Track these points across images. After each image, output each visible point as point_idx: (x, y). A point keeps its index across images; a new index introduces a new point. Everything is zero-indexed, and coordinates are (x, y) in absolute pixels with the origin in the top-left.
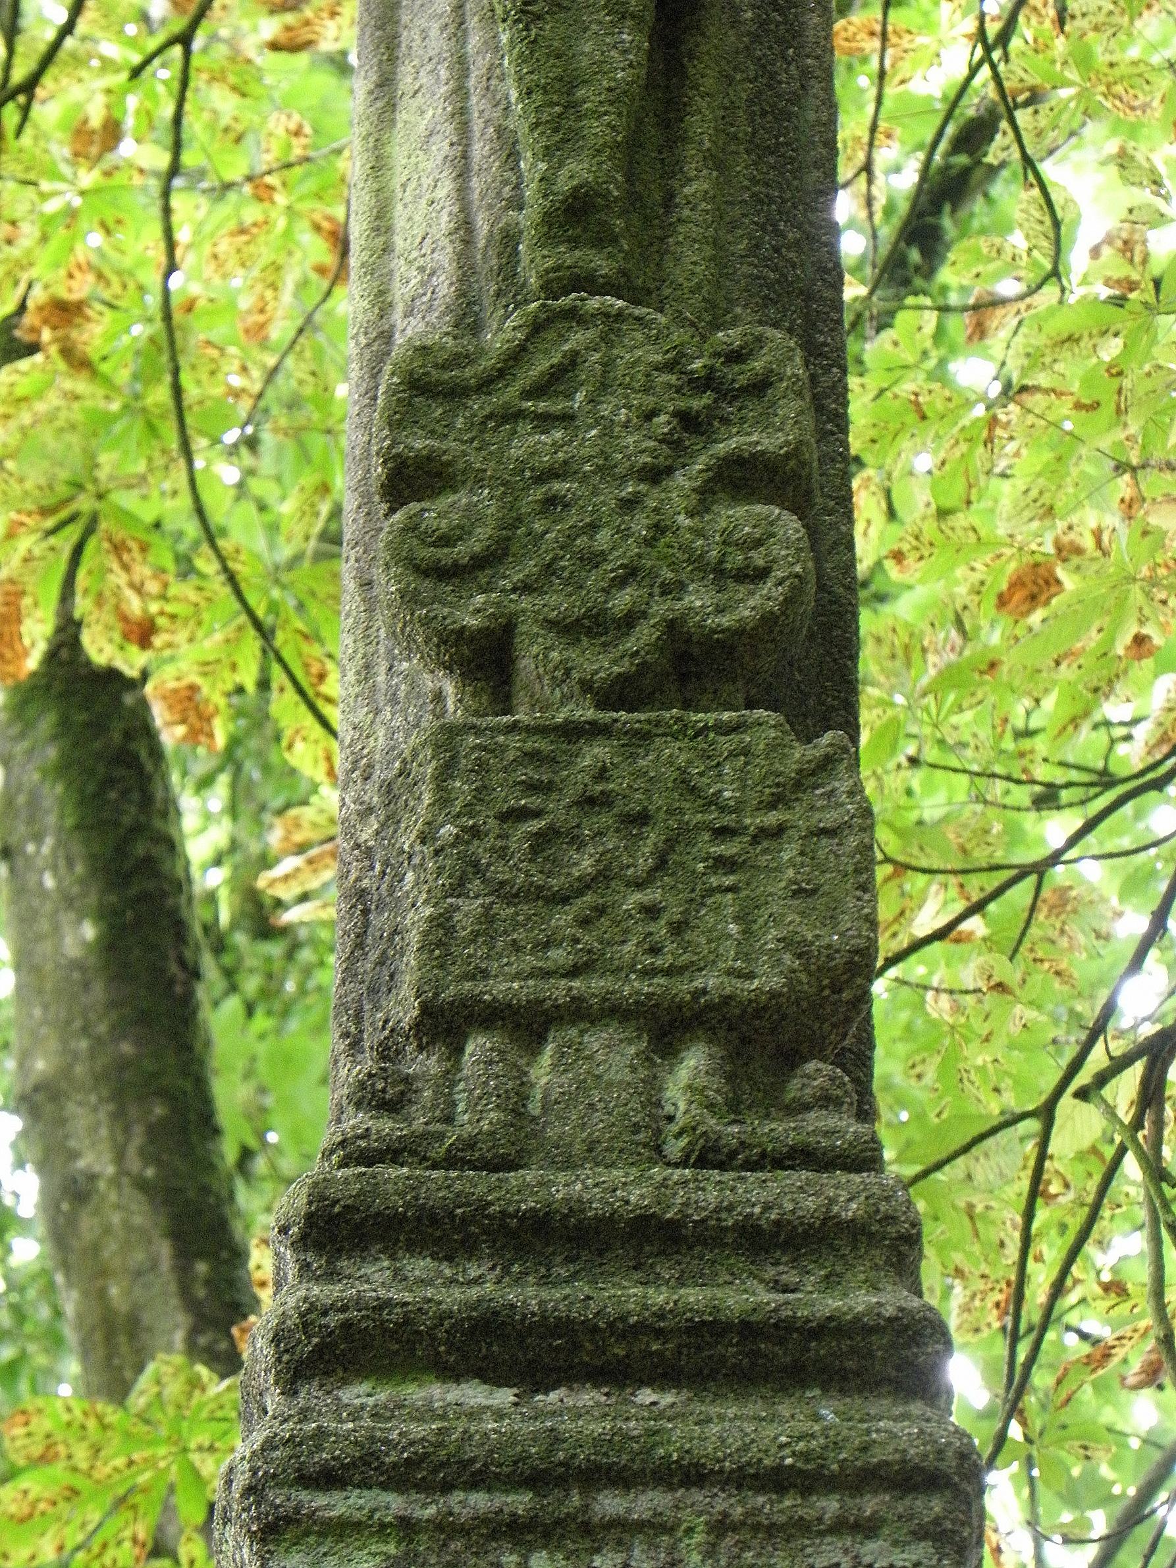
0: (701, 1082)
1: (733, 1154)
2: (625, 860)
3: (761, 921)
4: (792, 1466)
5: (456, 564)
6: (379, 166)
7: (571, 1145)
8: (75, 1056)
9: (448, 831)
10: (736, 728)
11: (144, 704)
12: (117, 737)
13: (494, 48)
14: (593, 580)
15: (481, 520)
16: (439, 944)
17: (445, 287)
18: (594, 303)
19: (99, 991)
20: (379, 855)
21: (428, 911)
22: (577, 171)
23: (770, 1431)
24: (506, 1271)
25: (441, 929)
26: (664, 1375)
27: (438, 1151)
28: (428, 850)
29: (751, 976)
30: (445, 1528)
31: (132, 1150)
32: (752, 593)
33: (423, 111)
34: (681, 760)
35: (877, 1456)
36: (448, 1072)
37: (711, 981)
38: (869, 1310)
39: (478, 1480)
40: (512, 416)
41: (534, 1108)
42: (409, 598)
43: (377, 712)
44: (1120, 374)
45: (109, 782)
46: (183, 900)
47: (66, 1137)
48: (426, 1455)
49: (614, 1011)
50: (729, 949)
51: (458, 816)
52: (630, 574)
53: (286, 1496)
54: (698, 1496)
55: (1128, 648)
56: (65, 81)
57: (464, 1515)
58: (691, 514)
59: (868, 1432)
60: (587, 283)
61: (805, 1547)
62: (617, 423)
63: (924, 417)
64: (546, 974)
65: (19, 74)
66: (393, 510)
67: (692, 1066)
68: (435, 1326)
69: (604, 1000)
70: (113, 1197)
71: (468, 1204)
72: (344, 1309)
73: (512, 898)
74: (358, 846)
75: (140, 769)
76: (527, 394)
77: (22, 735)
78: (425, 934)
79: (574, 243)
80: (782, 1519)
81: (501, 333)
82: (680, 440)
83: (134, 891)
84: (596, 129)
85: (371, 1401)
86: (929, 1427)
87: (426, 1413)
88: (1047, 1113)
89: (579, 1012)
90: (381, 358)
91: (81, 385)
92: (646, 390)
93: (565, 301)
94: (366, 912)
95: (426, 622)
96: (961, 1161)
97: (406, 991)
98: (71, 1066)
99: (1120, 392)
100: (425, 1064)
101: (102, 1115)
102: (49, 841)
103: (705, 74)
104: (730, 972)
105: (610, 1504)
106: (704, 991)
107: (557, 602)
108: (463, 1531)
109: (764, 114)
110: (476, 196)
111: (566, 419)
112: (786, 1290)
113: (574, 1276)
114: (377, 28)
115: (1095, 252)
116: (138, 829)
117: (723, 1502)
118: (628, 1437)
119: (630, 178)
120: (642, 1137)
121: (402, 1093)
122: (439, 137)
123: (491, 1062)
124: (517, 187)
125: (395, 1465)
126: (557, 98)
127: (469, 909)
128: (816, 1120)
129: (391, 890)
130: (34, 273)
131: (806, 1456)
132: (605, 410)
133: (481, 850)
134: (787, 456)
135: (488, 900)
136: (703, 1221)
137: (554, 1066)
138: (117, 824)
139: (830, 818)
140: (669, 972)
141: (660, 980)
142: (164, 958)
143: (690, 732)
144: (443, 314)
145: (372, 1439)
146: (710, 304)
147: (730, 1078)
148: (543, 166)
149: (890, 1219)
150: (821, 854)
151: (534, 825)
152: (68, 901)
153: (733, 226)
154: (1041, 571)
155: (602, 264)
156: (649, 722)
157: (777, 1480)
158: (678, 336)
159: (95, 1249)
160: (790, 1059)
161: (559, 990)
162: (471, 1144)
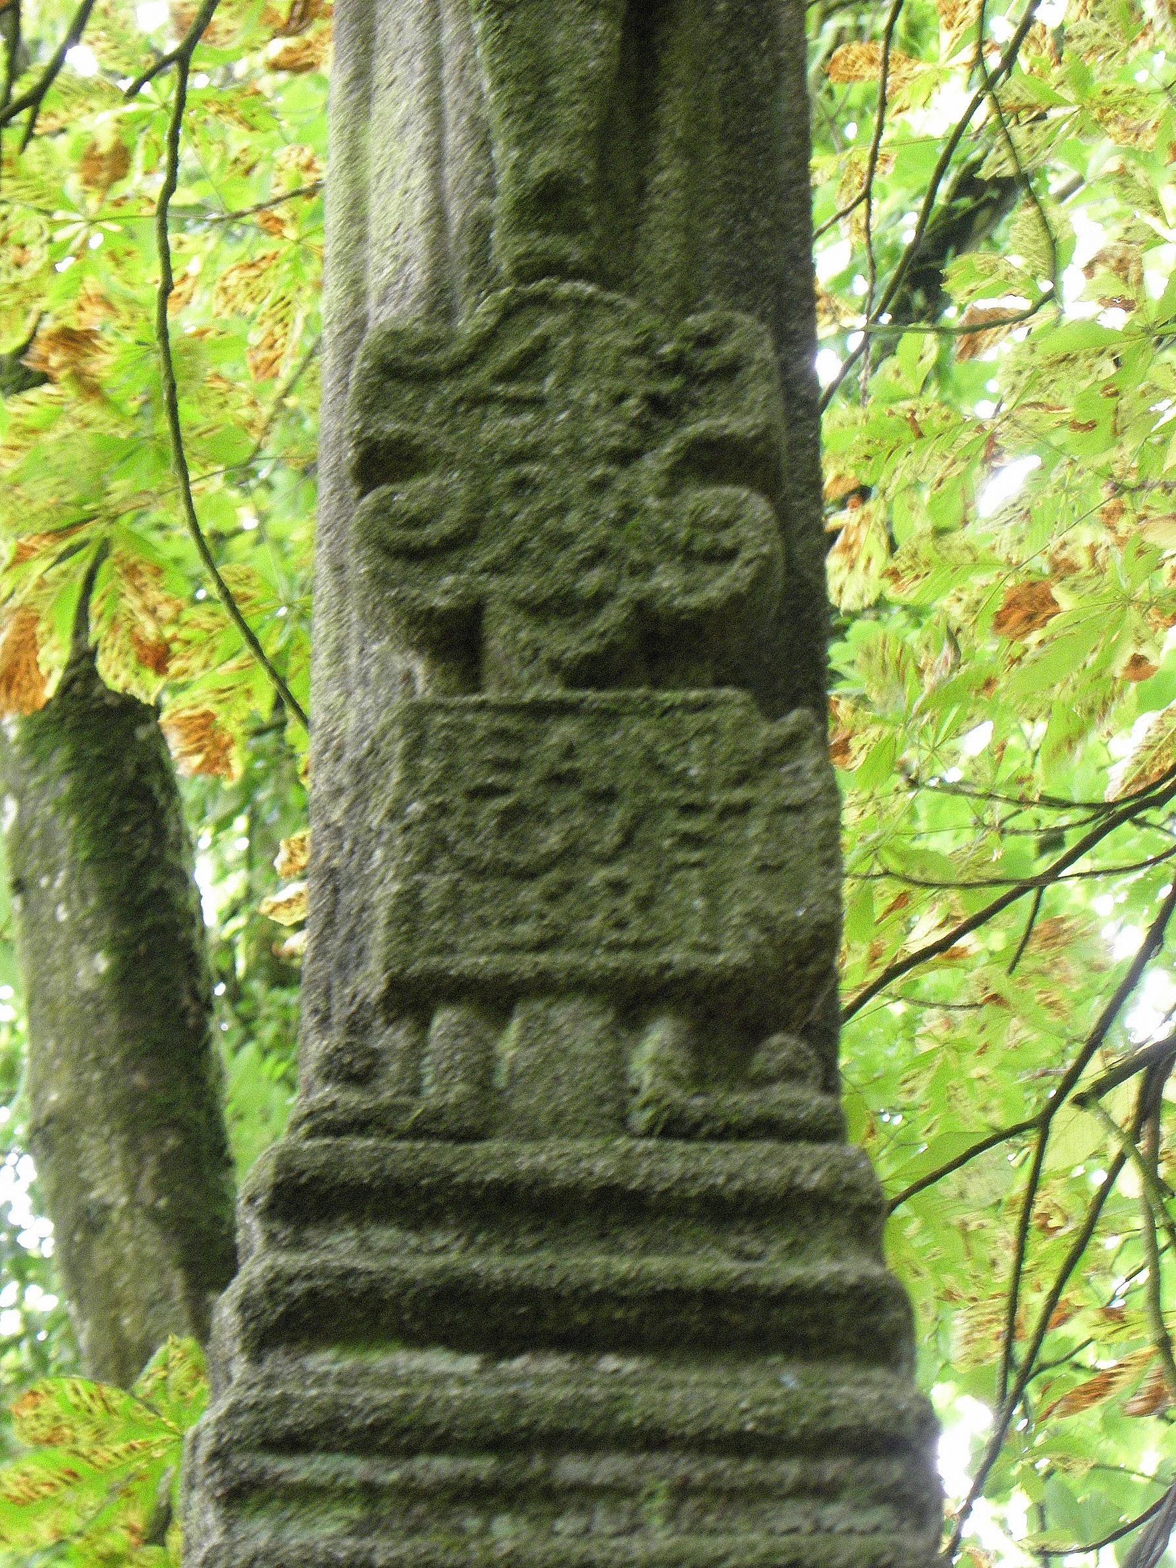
0: (667, 1054)
1: (698, 1126)
2: (592, 837)
3: (726, 897)
4: (752, 1432)
5: (425, 546)
6: (354, 157)
7: (535, 1117)
8: (88, 1088)
9: (416, 808)
11: (159, 737)
12: (130, 771)
13: (468, 37)
14: (563, 561)
15: (450, 502)
16: (406, 920)
17: (418, 274)
18: (565, 289)
19: (111, 1023)
20: (349, 833)
21: (396, 887)
22: (548, 159)
23: (732, 1396)
24: (471, 1242)
25: (409, 906)
26: (627, 1342)
27: (405, 1123)
28: (397, 826)
29: (716, 950)
30: (408, 1492)
31: (145, 1180)
32: (719, 574)
33: (399, 101)
34: (649, 737)
35: (838, 1421)
36: (414, 1047)
37: (677, 956)
38: (832, 1277)
39: (442, 1444)
40: (481, 400)
41: (501, 1080)
42: (380, 579)
43: (349, 694)
44: (1116, 394)
45: (122, 815)
46: (196, 932)
47: (79, 1169)
48: (389, 1422)
49: (581, 986)
50: (695, 925)
51: (426, 794)
52: (599, 555)
53: (252, 1469)
54: (660, 1461)
55: (1126, 669)
56: (76, 111)
58: (661, 495)
59: (828, 1397)
60: (558, 269)
61: (764, 1512)
62: (586, 408)
63: (920, 435)
64: (512, 949)
65: (20, 90)
66: (363, 494)
67: (659, 1037)
68: (399, 1295)
69: (570, 975)
70: (126, 1227)
71: (432, 1174)
72: (309, 1277)
73: (480, 874)
74: (327, 826)
75: (154, 801)
76: (499, 378)
77: (36, 768)
78: (394, 909)
79: (546, 230)
80: (742, 1483)
81: (473, 317)
82: (649, 424)
83: (147, 923)
85: (336, 1368)
86: (892, 1392)
87: (390, 1380)
88: (1043, 1123)
89: (545, 986)
90: (354, 345)
91: (91, 411)
92: (617, 373)
94: (336, 890)
95: (397, 602)
96: (952, 1175)
98: (83, 1098)
99: (1116, 411)
100: (392, 1038)
101: (114, 1147)
102: (62, 875)
103: (678, 63)
104: (696, 947)
105: (572, 1468)
106: (668, 966)
109: (736, 104)
110: (449, 184)
111: (536, 402)
112: (749, 1257)
113: (538, 1246)
114: (352, 23)
115: (1090, 269)
116: (150, 863)
117: (685, 1467)
118: (590, 1404)
119: (603, 167)
120: (608, 1108)
121: (369, 1067)
122: (413, 127)
123: (457, 1036)
124: (489, 175)
125: (359, 1431)
126: (529, 85)
127: (437, 884)
128: (781, 1092)
129: (361, 867)
130: (42, 304)
131: (767, 1421)
132: (575, 393)
133: (449, 827)
134: (756, 440)
135: (457, 876)
136: (666, 1192)
137: (521, 1039)
138: (129, 857)
139: (795, 795)
140: (637, 946)
141: (626, 955)
142: (176, 989)
143: (657, 711)
144: (415, 302)
145: (337, 1406)
146: (682, 291)
147: (697, 1051)
148: (515, 154)
149: (852, 1189)
150: (788, 830)
151: (502, 803)
152: (82, 934)
153: (706, 213)
154: (1037, 590)
155: (574, 251)
156: (615, 700)
157: (738, 1445)
158: (648, 321)
159: (109, 1278)
160: (755, 1033)
161: (526, 965)
162: (437, 1115)
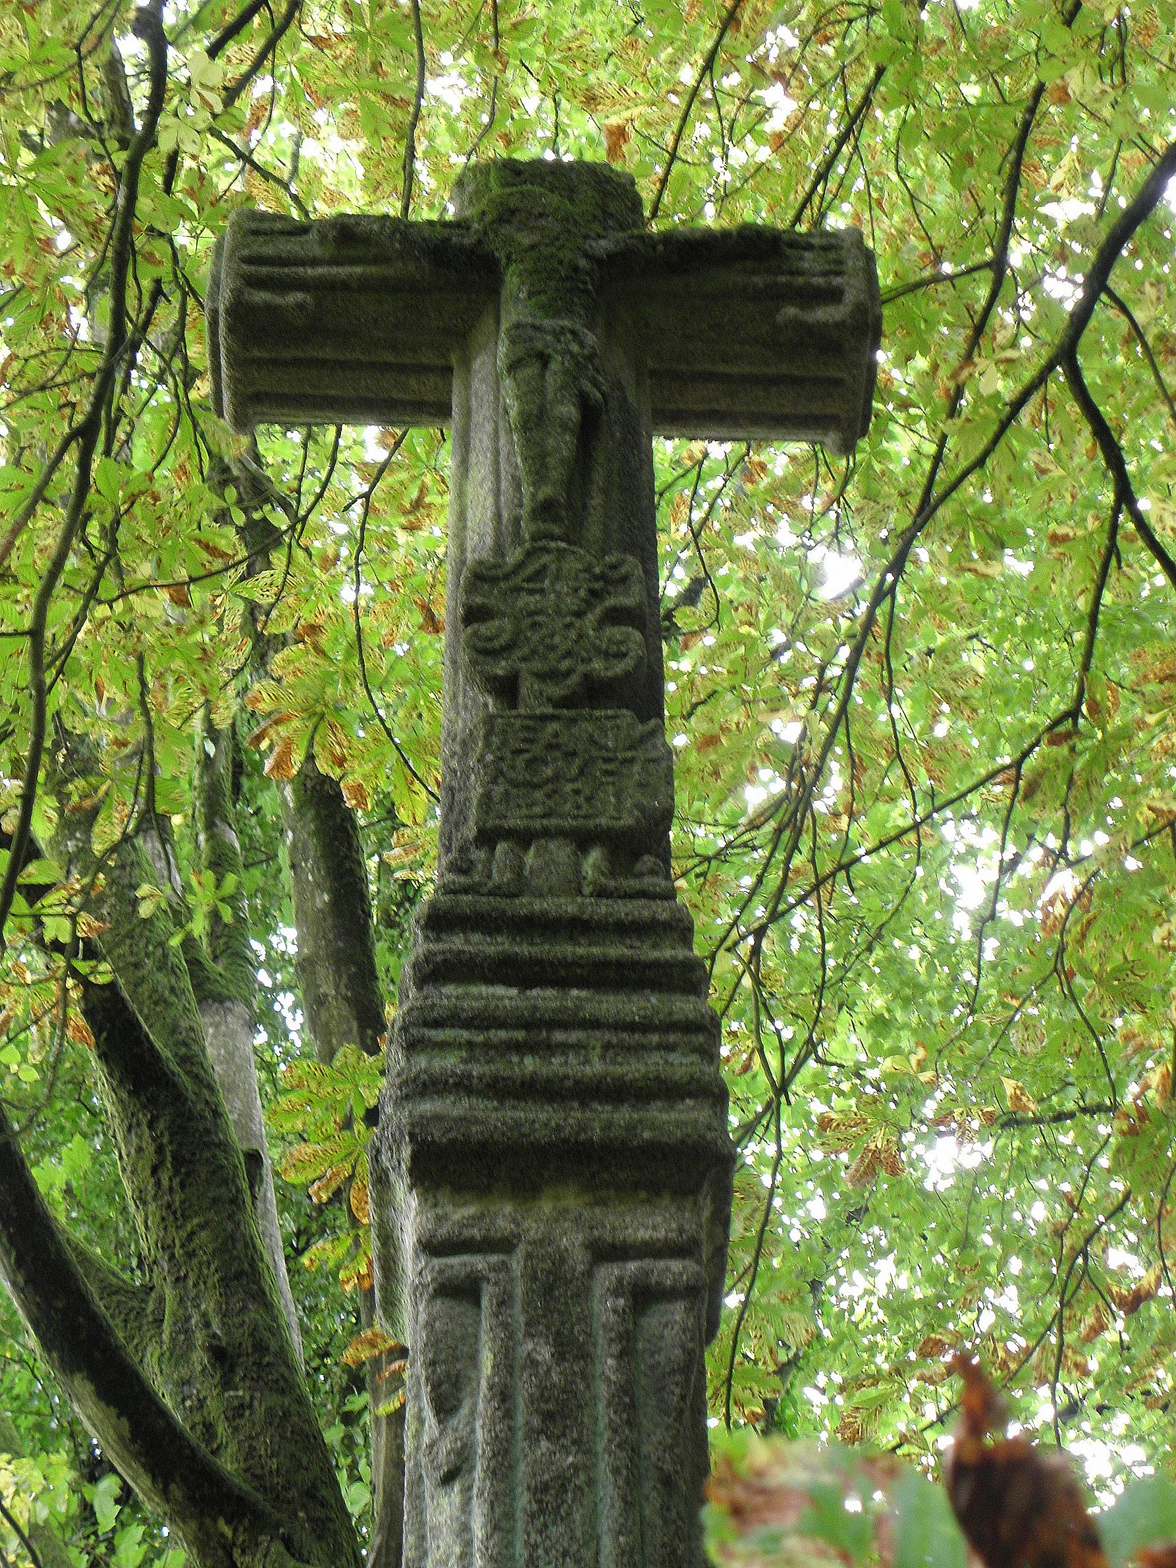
9: (489, 757)
10: (615, 717)
14: (552, 656)
17: (489, 541)
18: (553, 545)
19: (330, 921)
22: (546, 491)
25: (487, 798)
26: (582, 984)
27: (485, 890)
30: (487, 1045)
33: (481, 470)
35: (675, 1017)
37: (603, 821)
39: (502, 1025)
41: (526, 873)
42: (474, 663)
49: (561, 833)
52: (569, 654)
54: (598, 1034)
57: (495, 1040)
60: (552, 537)
62: (563, 593)
64: (530, 817)
73: (516, 785)
81: (513, 556)
84: (555, 475)
87: (480, 997)
89: (546, 833)
93: (541, 544)
97: (471, 823)
105: (559, 1036)
107: (537, 665)
108: (495, 1047)
111: (542, 591)
116: (346, 857)
117: (608, 1036)
126: (538, 462)
127: (498, 790)
139: (654, 755)
140: (586, 817)
151: (527, 756)
155: (557, 530)
157: (632, 1027)
160: (636, 856)
161: (537, 824)
162: (499, 887)
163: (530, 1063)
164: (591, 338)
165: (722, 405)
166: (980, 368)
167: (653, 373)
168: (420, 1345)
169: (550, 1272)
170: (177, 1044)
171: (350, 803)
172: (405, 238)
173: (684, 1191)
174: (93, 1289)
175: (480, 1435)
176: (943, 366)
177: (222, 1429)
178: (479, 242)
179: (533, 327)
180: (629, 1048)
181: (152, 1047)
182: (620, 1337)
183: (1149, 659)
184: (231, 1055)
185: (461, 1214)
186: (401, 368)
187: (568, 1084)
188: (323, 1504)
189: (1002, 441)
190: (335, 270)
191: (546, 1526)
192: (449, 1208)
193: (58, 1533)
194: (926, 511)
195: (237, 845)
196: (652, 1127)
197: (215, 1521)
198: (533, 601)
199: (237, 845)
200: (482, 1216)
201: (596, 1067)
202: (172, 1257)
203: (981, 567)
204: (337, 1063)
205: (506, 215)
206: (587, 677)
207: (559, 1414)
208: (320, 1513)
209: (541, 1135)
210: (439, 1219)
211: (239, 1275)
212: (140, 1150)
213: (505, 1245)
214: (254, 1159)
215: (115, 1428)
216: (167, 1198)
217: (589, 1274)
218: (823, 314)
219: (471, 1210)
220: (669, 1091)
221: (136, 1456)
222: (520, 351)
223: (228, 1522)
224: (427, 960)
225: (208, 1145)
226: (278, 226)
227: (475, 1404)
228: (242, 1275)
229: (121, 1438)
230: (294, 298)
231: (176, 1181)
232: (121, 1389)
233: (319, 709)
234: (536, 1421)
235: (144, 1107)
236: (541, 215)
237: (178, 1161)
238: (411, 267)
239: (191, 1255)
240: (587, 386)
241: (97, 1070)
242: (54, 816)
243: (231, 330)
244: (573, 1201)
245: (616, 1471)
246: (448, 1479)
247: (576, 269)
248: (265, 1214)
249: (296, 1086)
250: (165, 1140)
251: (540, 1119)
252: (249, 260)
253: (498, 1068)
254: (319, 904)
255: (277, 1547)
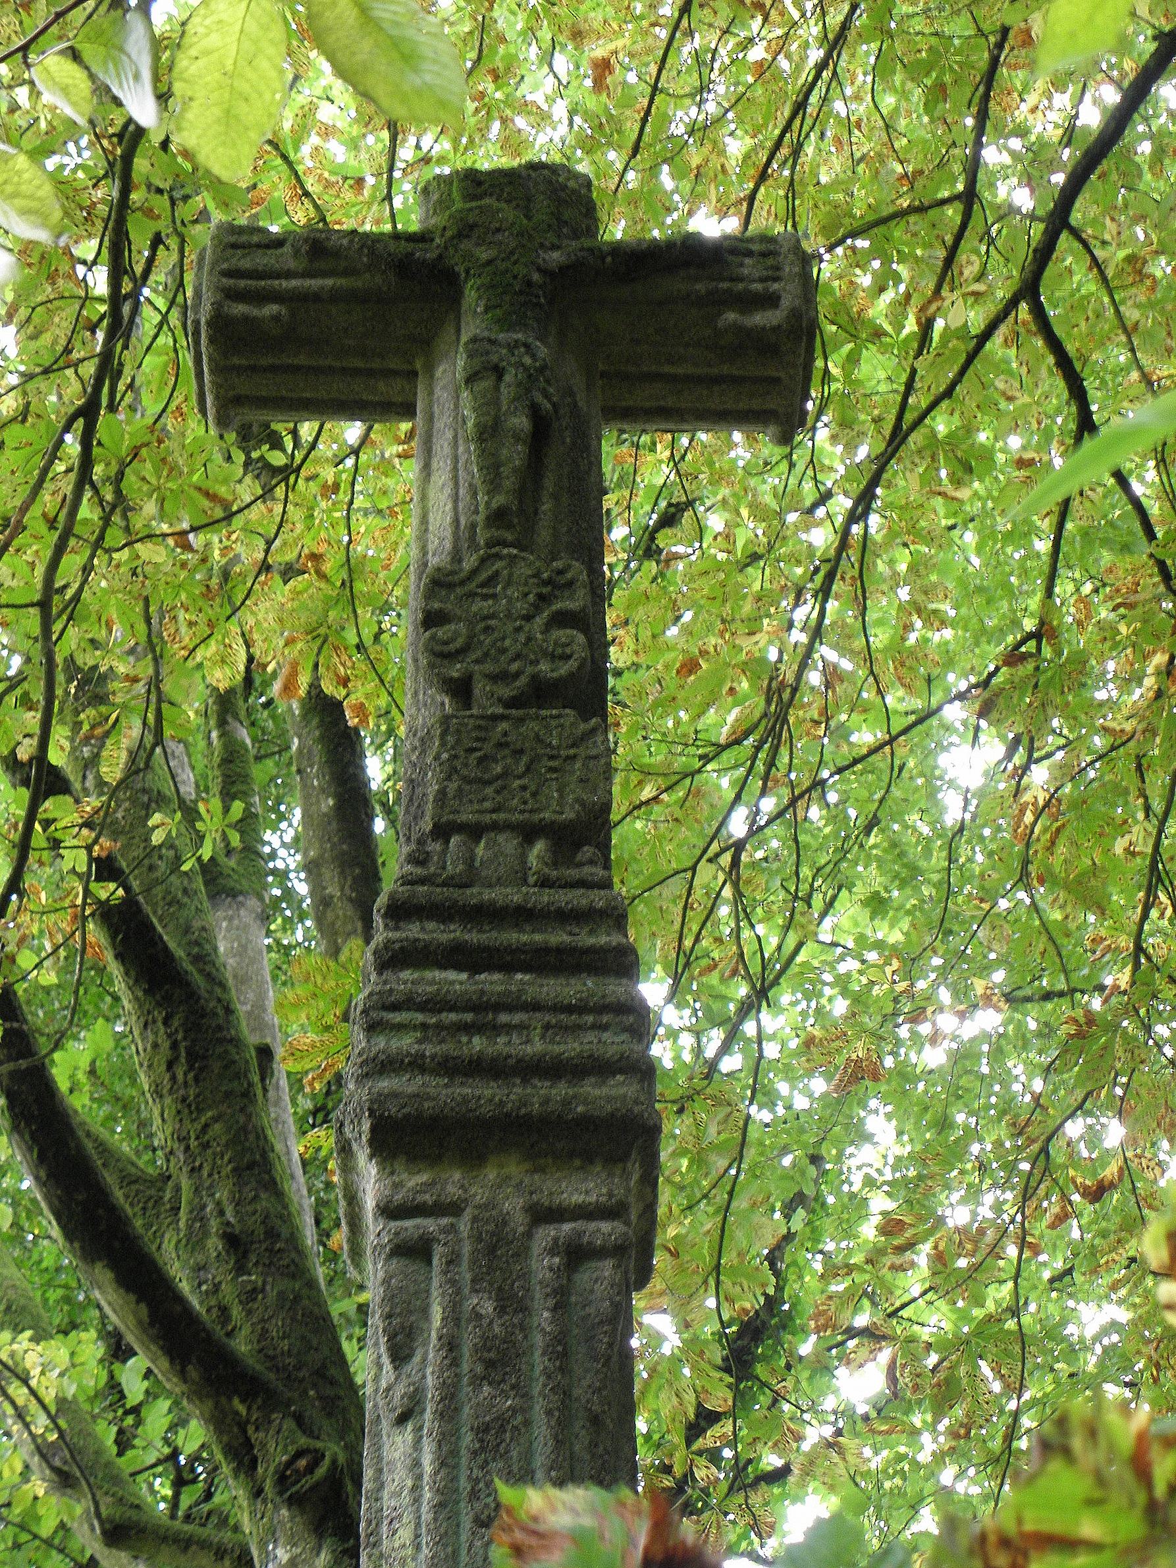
9: (445, 756)
10: (559, 716)
17: (448, 545)
19: (334, 825)
22: (499, 500)
25: (442, 795)
26: (526, 968)
30: (439, 1027)
33: (441, 476)
37: (547, 815)
39: (451, 1009)
42: (431, 666)
49: (508, 827)
52: (518, 656)
60: (505, 544)
62: (513, 598)
73: (470, 782)
81: (469, 562)
84: (507, 484)
87: (432, 982)
89: (495, 827)
97: (428, 818)
105: (504, 1018)
107: (489, 667)
117: (548, 1017)
126: (492, 470)
127: (453, 786)
139: (594, 752)
155: (509, 536)
157: (569, 1009)
160: (578, 846)
161: (487, 818)
163: (478, 1043)
164: (543, 351)
165: (670, 402)
166: (947, 303)
167: (603, 375)
168: (378, 1299)
169: (493, 1234)
170: (189, 943)
171: (352, 722)
172: (372, 253)
173: (615, 1158)
174: (110, 1178)
175: (430, 1381)
176: (915, 296)
177: (236, 1312)
178: (440, 257)
179: (490, 341)
180: (567, 1028)
181: (166, 948)
182: (555, 1292)
183: (1121, 573)
184: (244, 947)
185: (415, 1180)
186: (370, 373)
187: (511, 1062)
188: (333, 1382)
189: (970, 372)
190: (308, 282)
191: (486, 1462)
192: (405, 1176)
193: (86, 1407)
194: (897, 438)
195: (248, 741)
196: (585, 1102)
197: (230, 1399)
198: (485, 606)
199: (248, 741)
200: (433, 1183)
201: (537, 1046)
202: (187, 1148)
203: (949, 489)
204: (343, 958)
205: (465, 230)
206: (534, 678)
207: (499, 1362)
208: (329, 1391)
209: (486, 1110)
210: (396, 1186)
211: (251, 1166)
212: (155, 1046)
213: (454, 1209)
214: (265, 1053)
215: (135, 1313)
216: (182, 1092)
217: (529, 1235)
218: (761, 319)
219: (424, 1178)
220: (601, 1068)
221: (154, 1339)
222: (477, 362)
223: (243, 1401)
224: (386, 947)
225: (221, 1041)
226: (255, 239)
227: (426, 1353)
228: (255, 1165)
229: (140, 1322)
230: (272, 309)
231: (191, 1075)
232: (140, 1276)
233: (322, 631)
234: (479, 1369)
235: (159, 1004)
236: (498, 230)
237: (192, 1057)
238: (378, 279)
239: (206, 1146)
240: (539, 398)
241: (115, 969)
242: (67, 744)
243: (211, 340)
244: (515, 1168)
245: (549, 1413)
246: (402, 1420)
247: (529, 284)
248: (278, 1102)
249: (302, 994)
250: (180, 1036)
251: (485, 1094)
252: (228, 274)
253: (447, 1048)
254: (324, 808)
255: (289, 1424)
